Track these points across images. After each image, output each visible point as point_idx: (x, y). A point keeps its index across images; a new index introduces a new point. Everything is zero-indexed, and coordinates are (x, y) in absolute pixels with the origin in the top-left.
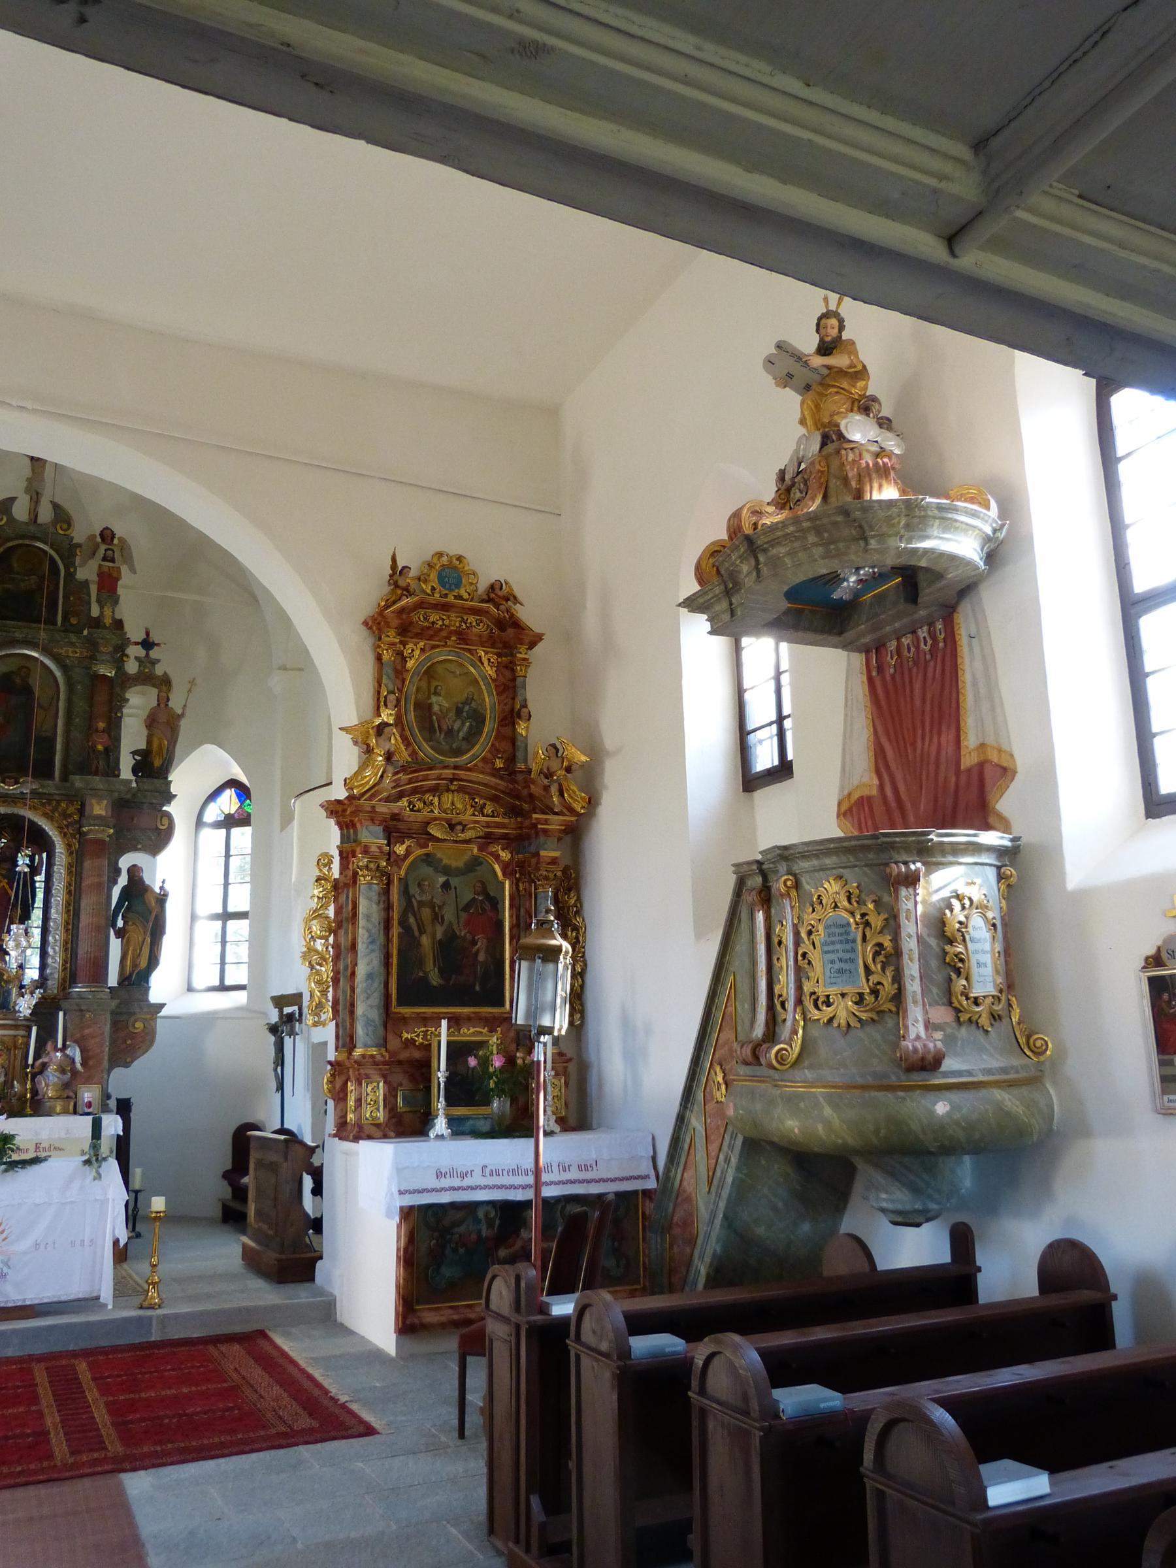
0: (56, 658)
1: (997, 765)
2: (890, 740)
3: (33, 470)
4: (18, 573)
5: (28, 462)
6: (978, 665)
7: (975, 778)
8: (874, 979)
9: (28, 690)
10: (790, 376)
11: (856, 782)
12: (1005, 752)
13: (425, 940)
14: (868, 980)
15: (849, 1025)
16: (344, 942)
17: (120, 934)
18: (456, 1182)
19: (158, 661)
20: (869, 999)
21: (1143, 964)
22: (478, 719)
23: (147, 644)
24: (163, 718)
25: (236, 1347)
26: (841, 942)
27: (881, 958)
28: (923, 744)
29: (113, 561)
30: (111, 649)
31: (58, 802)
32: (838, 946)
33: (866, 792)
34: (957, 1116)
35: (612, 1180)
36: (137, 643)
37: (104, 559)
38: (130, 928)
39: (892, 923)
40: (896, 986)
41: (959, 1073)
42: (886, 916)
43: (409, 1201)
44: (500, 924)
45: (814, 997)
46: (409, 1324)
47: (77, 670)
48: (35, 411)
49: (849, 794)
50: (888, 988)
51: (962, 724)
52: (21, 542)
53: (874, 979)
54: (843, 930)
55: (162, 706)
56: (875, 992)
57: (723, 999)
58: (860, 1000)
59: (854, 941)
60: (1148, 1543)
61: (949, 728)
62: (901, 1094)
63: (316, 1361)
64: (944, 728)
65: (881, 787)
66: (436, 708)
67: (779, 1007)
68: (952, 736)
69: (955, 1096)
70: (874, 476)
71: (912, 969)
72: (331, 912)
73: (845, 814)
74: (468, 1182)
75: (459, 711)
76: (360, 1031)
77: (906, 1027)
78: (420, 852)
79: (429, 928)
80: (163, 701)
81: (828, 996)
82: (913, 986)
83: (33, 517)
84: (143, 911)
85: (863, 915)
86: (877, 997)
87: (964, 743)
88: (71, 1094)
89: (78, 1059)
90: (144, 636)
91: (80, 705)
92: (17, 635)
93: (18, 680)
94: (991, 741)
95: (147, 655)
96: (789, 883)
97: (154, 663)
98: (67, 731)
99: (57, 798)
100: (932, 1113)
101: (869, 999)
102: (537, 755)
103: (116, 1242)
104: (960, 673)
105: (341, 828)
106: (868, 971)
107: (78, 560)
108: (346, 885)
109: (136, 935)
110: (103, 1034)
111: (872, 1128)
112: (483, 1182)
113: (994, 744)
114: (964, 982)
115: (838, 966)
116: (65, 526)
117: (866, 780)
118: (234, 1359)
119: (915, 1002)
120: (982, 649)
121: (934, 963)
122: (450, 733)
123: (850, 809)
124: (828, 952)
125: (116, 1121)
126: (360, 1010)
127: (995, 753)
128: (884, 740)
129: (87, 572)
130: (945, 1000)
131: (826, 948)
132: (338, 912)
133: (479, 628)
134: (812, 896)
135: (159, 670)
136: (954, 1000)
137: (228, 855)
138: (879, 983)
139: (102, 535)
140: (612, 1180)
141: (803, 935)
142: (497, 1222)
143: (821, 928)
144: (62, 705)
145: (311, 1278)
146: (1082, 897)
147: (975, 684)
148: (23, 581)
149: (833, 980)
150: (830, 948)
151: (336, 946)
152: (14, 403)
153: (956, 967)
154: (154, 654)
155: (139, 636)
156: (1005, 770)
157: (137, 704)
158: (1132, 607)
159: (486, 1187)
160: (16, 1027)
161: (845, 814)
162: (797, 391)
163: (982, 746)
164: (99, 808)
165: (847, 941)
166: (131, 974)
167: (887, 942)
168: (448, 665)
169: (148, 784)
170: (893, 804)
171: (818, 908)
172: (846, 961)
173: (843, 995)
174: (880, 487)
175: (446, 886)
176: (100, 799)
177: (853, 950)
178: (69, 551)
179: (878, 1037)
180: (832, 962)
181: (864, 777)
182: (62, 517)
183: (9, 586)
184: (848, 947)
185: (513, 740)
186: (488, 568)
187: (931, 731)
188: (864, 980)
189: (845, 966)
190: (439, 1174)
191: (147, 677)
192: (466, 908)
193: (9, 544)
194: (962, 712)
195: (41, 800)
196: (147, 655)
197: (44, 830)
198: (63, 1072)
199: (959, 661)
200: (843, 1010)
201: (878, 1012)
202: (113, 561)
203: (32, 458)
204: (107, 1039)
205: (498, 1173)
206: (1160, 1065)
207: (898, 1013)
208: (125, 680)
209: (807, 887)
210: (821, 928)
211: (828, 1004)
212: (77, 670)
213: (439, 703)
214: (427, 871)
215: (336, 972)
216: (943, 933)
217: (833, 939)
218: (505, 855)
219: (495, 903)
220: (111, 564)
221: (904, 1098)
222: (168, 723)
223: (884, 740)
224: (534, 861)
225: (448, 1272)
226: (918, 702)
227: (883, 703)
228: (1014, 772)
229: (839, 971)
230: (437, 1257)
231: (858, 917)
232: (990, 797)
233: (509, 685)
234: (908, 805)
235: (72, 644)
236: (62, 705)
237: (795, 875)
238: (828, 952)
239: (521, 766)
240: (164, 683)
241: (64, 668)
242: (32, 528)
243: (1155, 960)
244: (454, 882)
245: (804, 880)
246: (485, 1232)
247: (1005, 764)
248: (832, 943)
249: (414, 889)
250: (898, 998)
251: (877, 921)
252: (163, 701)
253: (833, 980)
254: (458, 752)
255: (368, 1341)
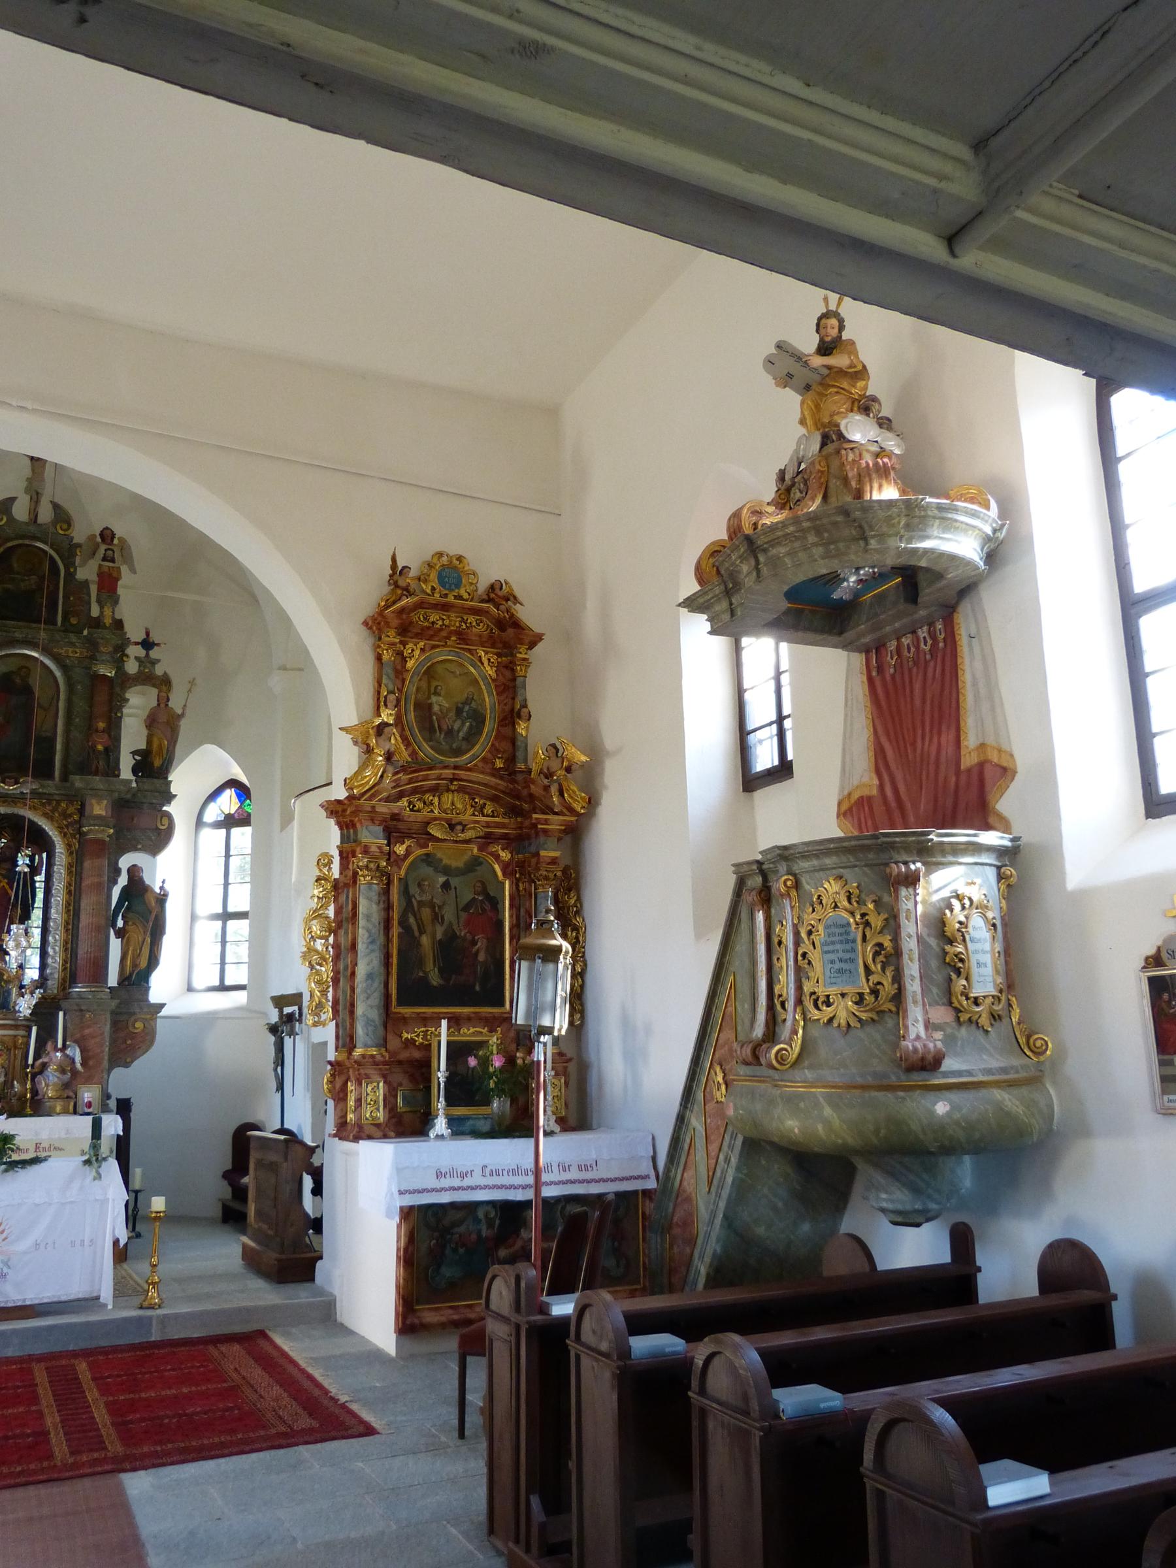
0: (56, 658)
1: (997, 765)
2: (890, 740)
3: (33, 470)
4: (18, 573)
5: (28, 462)
6: (978, 665)
7: (975, 778)
8: (874, 979)
9: (28, 690)
10: (790, 376)
11: (856, 782)
12: (1005, 752)
13: (425, 940)
14: (868, 980)
15: (849, 1025)
16: (344, 942)
17: (120, 934)
18: (456, 1182)
19: (158, 661)
20: (869, 999)
21: (1143, 964)
22: (478, 719)
23: (147, 644)
24: (163, 718)
25: (236, 1347)
26: (841, 942)
27: (881, 958)
28: (923, 744)
29: (113, 561)
30: (111, 649)
31: (58, 802)
32: (838, 946)
33: (866, 792)
34: (957, 1116)
35: (612, 1180)
36: (137, 643)
37: (104, 559)
38: (130, 928)
39: (892, 923)
40: (896, 986)
41: (959, 1073)
42: (886, 916)
43: (409, 1201)
44: (500, 924)
45: (814, 997)
46: (409, 1324)
47: (77, 670)
48: (35, 411)
49: (849, 794)
50: (888, 988)
51: (962, 724)
52: (21, 542)
53: (874, 979)
54: (843, 930)
55: (162, 706)
56: (875, 992)
57: (723, 999)
58: (860, 1000)
59: (854, 941)
60: (1148, 1543)
61: (949, 728)
62: (901, 1094)
63: (316, 1361)
64: (944, 728)
65: (881, 787)
66: (436, 708)
67: (779, 1007)
68: (952, 736)
69: (955, 1096)
70: (874, 476)
71: (912, 969)
72: (331, 912)
73: (845, 814)
74: (468, 1182)
75: (459, 711)
76: (360, 1031)
77: (906, 1027)
78: (420, 852)
79: (429, 928)
80: (163, 701)
81: (828, 996)
82: (913, 986)
83: (33, 517)
84: (143, 911)
85: (863, 915)
86: (877, 997)
87: (964, 743)
88: (71, 1094)
89: (78, 1059)
90: (144, 636)
91: (80, 705)
92: (17, 635)
93: (18, 680)
94: (991, 741)
95: (147, 655)
96: (789, 883)
97: (154, 663)
98: (67, 731)
99: (57, 798)
100: (932, 1113)
101: (869, 999)
102: (537, 755)
103: (116, 1242)
104: (960, 673)
105: (341, 828)
106: (868, 971)
107: (78, 560)
108: (346, 885)
109: (136, 935)
110: (103, 1034)
111: (872, 1128)
112: (483, 1182)
113: (994, 744)
114: (964, 982)
115: (838, 966)
116: (65, 526)
117: (866, 780)
118: (234, 1359)
119: (915, 1002)
120: (982, 649)
121: (934, 963)
122: (450, 733)
123: (850, 809)
124: (828, 952)
125: (116, 1121)
126: (360, 1010)
127: (995, 753)
128: (884, 740)
129: (87, 572)
130: (945, 1000)
131: (826, 948)
132: (338, 912)
133: (479, 628)
134: (812, 896)
135: (159, 670)
136: (954, 1000)
137: (228, 855)
138: (879, 983)
139: (102, 535)
140: (612, 1180)
141: (803, 935)
142: (497, 1222)
143: (821, 928)
144: (62, 705)
145: (311, 1278)
146: (1082, 897)
147: (975, 684)
148: (23, 581)
149: (833, 980)
150: (830, 948)
151: (336, 946)
152: (14, 403)
153: (956, 967)
154: (154, 654)
155: (139, 636)
156: (1005, 770)
157: (137, 704)
158: (1132, 607)
159: (486, 1187)
160: (16, 1027)
161: (845, 814)
162: (797, 391)
163: (982, 746)
164: (99, 808)
165: (847, 941)
166: (131, 974)
167: (887, 942)
168: (448, 665)
169: (148, 784)
170: (893, 804)
171: (818, 908)
172: (846, 961)
173: (843, 995)
174: (880, 487)
175: (446, 886)
176: (100, 799)
177: (853, 950)
178: (69, 551)
179: (878, 1037)
180: (832, 962)
181: (864, 777)
182: (62, 517)
183: (9, 586)
184: (848, 947)
185: (513, 740)
186: (488, 568)
187: (931, 731)
188: (864, 980)
189: (845, 966)
190: (439, 1174)
191: (147, 677)
192: (466, 908)
193: (9, 544)
194: (962, 712)
195: (41, 800)
196: (147, 655)
197: (44, 830)
198: (63, 1072)
199: (959, 661)
200: (843, 1010)
201: (878, 1012)
202: (113, 561)
203: (32, 458)
204: (107, 1039)
205: (498, 1173)
206: (1160, 1065)
207: (898, 1013)
208: (125, 680)
209: (807, 887)
210: (821, 928)
211: (828, 1004)
212: (77, 670)
213: (439, 703)
214: (427, 871)
215: (336, 972)
216: (943, 933)
217: (833, 939)
218: (505, 855)
219: (495, 903)
220: (111, 564)
221: (904, 1098)
222: (168, 723)
223: (884, 740)
224: (534, 861)
225: (448, 1272)
226: (918, 702)
227: (883, 703)
228: (1014, 772)
229: (839, 971)
230: (437, 1257)
231: (858, 917)
232: (990, 797)
233: (509, 685)
234: (908, 805)
235: (72, 644)
236: (62, 705)
237: (795, 875)
238: (828, 952)
239: (521, 766)
240: (164, 683)
241: (64, 668)
242: (32, 528)
243: (1155, 960)
244: (454, 882)
245: (804, 880)
246: (485, 1232)
247: (1005, 764)
248: (832, 943)
249: (414, 889)
250: (898, 998)
251: (877, 921)
252: (163, 701)
253: (833, 980)
254: (458, 752)
255: (368, 1341)
